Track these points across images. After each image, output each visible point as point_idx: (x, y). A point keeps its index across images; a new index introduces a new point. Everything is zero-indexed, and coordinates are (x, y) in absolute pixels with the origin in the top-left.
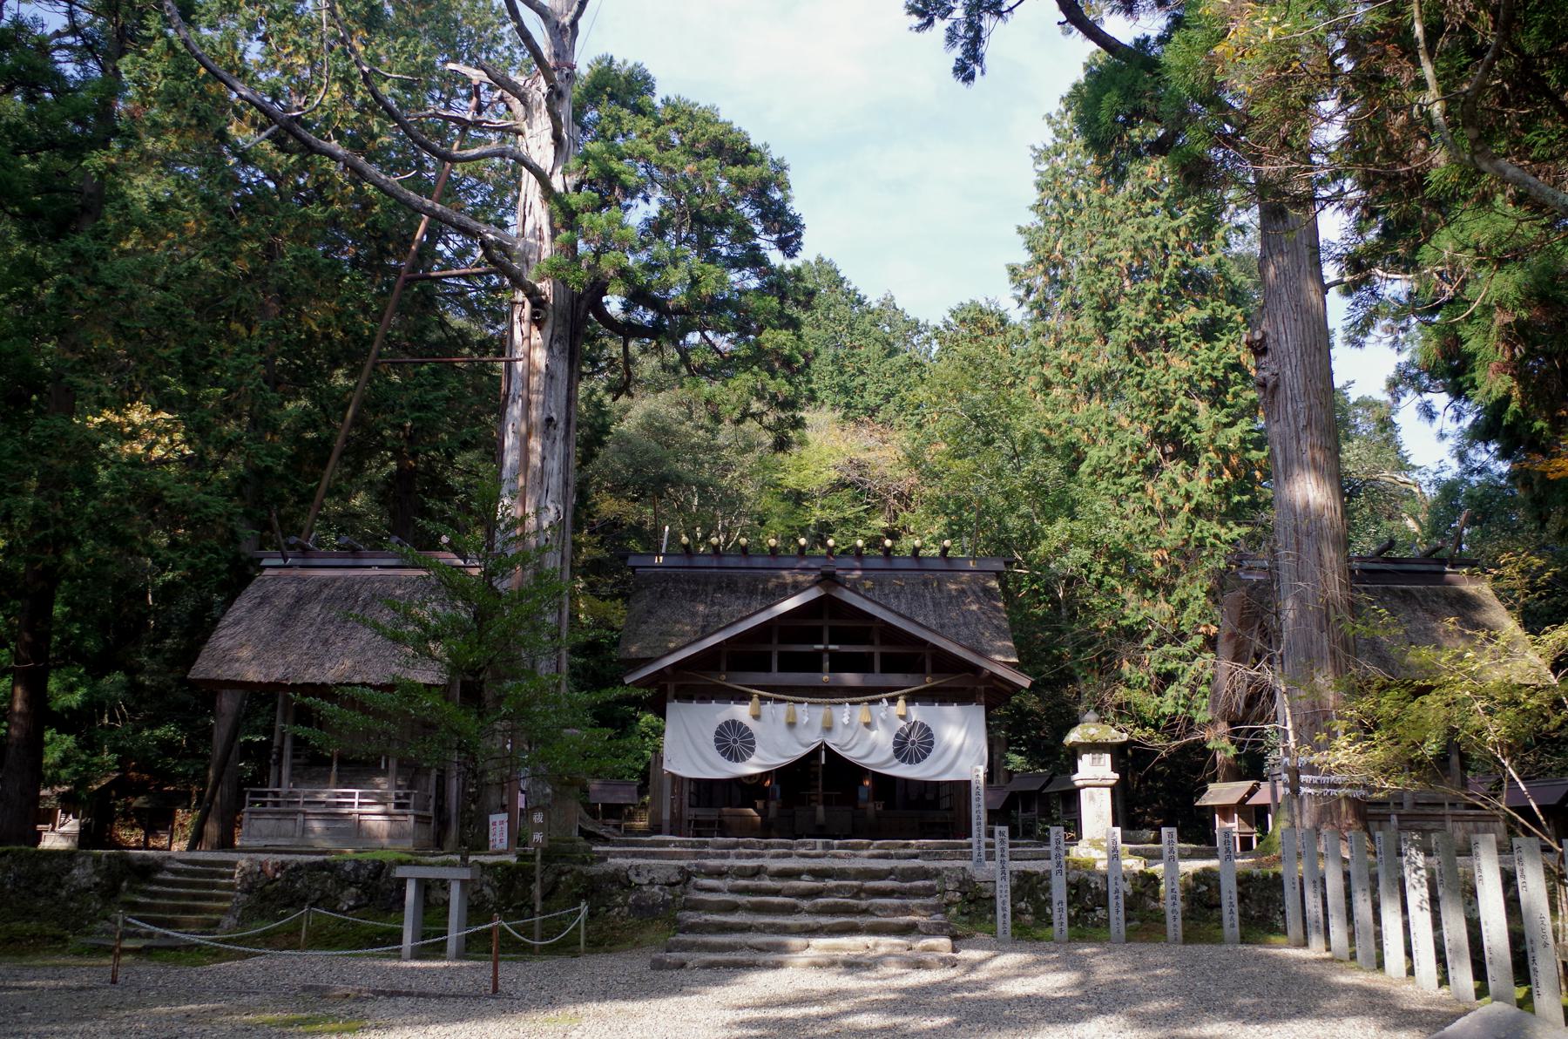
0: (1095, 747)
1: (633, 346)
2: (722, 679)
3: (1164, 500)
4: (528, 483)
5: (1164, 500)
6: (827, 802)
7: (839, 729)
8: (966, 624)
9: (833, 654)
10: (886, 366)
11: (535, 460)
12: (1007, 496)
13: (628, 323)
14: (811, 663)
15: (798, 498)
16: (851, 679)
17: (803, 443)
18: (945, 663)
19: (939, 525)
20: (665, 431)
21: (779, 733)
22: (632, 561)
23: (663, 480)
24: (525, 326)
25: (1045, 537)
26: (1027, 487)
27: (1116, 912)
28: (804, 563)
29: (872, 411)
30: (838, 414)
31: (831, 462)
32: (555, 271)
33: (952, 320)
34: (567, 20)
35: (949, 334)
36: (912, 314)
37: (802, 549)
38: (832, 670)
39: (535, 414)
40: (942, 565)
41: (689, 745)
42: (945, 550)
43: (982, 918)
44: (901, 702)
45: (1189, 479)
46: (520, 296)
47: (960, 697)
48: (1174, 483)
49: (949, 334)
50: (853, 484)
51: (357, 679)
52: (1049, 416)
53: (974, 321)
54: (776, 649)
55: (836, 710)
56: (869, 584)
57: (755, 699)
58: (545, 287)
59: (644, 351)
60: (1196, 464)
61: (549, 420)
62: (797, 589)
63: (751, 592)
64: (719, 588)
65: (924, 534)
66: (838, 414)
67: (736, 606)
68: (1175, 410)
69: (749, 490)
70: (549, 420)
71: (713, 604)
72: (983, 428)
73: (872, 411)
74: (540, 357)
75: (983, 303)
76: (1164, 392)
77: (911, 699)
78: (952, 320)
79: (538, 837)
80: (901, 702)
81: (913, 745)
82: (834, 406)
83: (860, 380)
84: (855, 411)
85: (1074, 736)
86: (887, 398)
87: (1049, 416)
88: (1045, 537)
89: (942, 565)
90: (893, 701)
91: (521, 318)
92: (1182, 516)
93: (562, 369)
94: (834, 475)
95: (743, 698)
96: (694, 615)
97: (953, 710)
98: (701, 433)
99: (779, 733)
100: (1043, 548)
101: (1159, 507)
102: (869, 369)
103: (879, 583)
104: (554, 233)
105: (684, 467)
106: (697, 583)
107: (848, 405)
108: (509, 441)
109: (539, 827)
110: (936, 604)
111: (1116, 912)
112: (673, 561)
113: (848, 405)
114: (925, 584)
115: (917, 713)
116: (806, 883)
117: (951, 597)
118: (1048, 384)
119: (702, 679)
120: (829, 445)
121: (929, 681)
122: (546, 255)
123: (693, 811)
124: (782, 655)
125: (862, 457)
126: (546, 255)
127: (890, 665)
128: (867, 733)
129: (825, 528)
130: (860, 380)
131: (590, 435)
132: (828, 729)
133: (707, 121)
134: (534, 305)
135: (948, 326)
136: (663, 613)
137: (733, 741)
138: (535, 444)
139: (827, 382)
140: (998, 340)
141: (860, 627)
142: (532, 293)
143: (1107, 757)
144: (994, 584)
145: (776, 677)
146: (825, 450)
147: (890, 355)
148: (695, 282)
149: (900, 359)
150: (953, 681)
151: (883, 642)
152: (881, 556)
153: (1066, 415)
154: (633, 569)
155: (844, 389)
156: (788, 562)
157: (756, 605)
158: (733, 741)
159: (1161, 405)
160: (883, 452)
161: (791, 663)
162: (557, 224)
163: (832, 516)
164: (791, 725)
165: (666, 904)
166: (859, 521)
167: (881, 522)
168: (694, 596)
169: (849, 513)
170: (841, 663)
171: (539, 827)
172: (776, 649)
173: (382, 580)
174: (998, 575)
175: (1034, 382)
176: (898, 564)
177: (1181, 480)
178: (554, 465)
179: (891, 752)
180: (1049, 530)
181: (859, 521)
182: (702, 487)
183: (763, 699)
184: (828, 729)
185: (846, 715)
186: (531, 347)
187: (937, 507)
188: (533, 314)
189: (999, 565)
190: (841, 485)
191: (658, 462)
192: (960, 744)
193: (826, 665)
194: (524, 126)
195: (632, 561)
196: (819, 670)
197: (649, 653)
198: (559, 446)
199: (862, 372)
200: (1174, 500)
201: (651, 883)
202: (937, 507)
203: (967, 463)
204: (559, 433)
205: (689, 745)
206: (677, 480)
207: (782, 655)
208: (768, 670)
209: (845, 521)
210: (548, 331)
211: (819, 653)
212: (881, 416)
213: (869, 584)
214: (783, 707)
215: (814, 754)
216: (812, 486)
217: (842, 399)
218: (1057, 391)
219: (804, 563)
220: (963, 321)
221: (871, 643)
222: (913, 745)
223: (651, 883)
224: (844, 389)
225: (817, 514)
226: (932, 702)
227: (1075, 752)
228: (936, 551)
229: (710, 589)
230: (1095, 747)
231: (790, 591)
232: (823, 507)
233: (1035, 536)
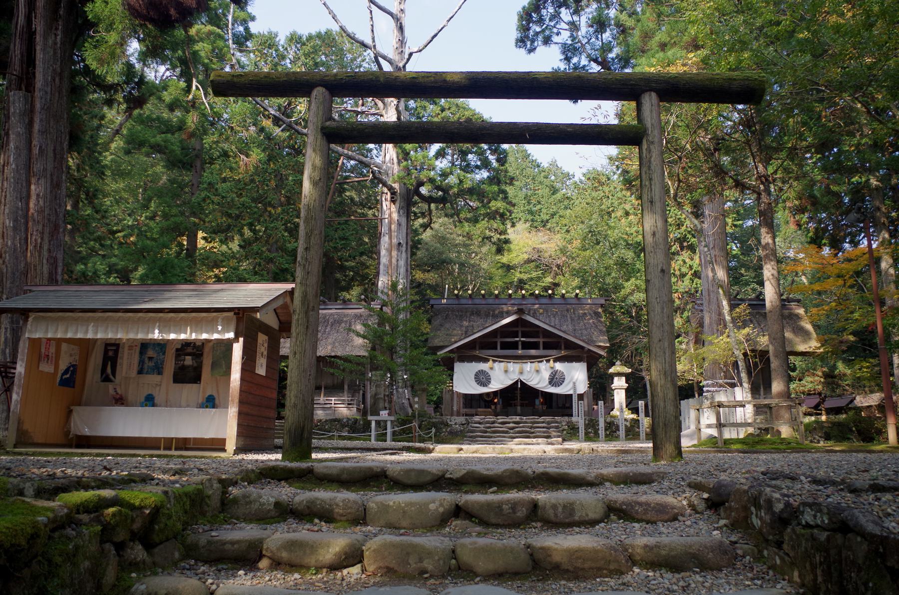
0: (619, 374)
1: (433, 206)
2: (477, 353)
3: (680, 270)
4: (391, 268)
5: (680, 270)
6: (522, 405)
7: (525, 373)
8: (586, 329)
9: (523, 342)
10: (551, 200)
11: (394, 261)
12: (606, 268)
13: (430, 197)
14: (514, 346)
15: (508, 268)
16: (533, 352)
17: (509, 250)
18: (569, 345)
19: (576, 282)
20: (443, 238)
21: (502, 375)
22: (432, 302)
23: (444, 262)
24: (388, 203)
25: (624, 288)
26: (616, 264)
27: (622, 433)
28: (512, 302)
29: (544, 223)
30: (528, 225)
31: (525, 250)
32: (401, 179)
33: (583, 178)
34: (401, 65)
35: (581, 186)
36: (566, 169)
37: (510, 295)
38: (523, 349)
39: (395, 241)
40: (575, 301)
41: (465, 380)
42: (577, 294)
43: (575, 435)
44: (552, 361)
45: (692, 259)
46: (386, 190)
47: (577, 359)
48: (684, 262)
49: (581, 186)
50: (536, 261)
51: (333, 354)
52: (627, 229)
53: (594, 179)
54: (499, 341)
55: (524, 365)
56: (541, 311)
57: (491, 361)
58: (396, 186)
59: (437, 209)
60: (694, 252)
61: (400, 244)
62: (509, 314)
63: (487, 315)
64: (472, 314)
65: (569, 286)
66: (528, 225)
67: (480, 321)
68: (684, 228)
69: (484, 265)
70: (400, 244)
71: (470, 321)
72: (594, 238)
73: (544, 223)
74: (395, 216)
75: (599, 169)
76: (679, 219)
77: (555, 360)
78: (583, 178)
79: (416, 406)
80: (552, 361)
81: (556, 379)
82: (526, 221)
83: (539, 207)
84: (538, 224)
85: (611, 370)
86: (553, 215)
87: (627, 229)
88: (624, 288)
89: (575, 301)
90: (548, 361)
91: (386, 200)
92: (688, 277)
93: (404, 221)
94: (526, 256)
95: (486, 360)
96: (462, 326)
97: (575, 365)
98: (461, 238)
99: (502, 375)
100: (623, 292)
101: (677, 273)
102: (543, 201)
103: (546, 311)
104: (399, 162)
105: (453, 256)
106: (462, 311)
107: (532, 220)
108: (383, 252)
109: (417, 403)
110: (572, 320)
111: (622, 433)
112: (450, 302)
113: (532, 220)
114: (567, 310)
115: (559, 366)
116: (512, 425)
117: (579, 317)
118: (627, 214)
119: (469, 353)
120: (523, 240)
121: (563, 353)
122: (396, 171)
123: (465, 410)
124: (502, 343)
125: (539, 246)
126: (396, 171)
127: (547, 346)
128: (537, 374)
129: (521, 283)
130: (539, 207)
131: (414, 245)
132: (521, 373)
133: (464, 108)
134: (392, 194)
135: (581, 182)
136: (447, 325)
137: (482, 378)
138: (394, 253)
139: (522, 208)
140: (606, 189)
141: (536, 331)
142: (390, 189)
143: (624, 378)
144: (600, 310)
145: (499, 352)
146: (521, 244)
147: (553, 194)
148: (461, 181)
149: (558, 196)
150: (572, 352)
151: (543, 337)
152: (548, 296)
153: (635, 228)
154: (432, 306)
155: (531, 212)
156: (504, 301)
157: (489, 321)
158: (482, 378)
159: (678, 225)
160: (549, 244)
161: (505, 346)
162: (400, 157)
163: (525, 277)
164: (506, 371)
165: (461, 431)
166: (539, 279)
167: (549, 280)
168: (461, 318)
169: (534, 274)
170: (526, 346)
171: (417, 403)
172: (499, 341)
173: (337, 314)
174: (602, 306)
175: (620, 213)
176: (555, 301)
177: (687, 260)
178: (402, 263)
179: (547, 382)
180: (626, 284)
181: (539, 279)
182: (462, 265)
183: (494, 361)
184: (521, 373)
185: (528, 366)
186: (390, 211)
187: (575, 273)
188: (392, 198)
189: (603, 301)
190: (529, 261)
191: (441, 253)
192: (576, 378)
193: (520, 347)
194: (384, 113)
195: (432, 302)
196: (517, 349)
197: (442, 344)
198: (404, 255)
199: (539, 203)
200: (684, 270)
201: (456, 424)
202: (575, 273)
203: (588, 253)
204: (404, 249)
205: (465, 380)
206: (451, 262)
207: (502, 343)
208: (496, 349)
209: (531, 279)
210: (398, 204)
211: (517, 342)
212: (549, 225)
213: (541, 311)
214: (502, 364)
215: (517, 382)
216: (515, 262)
217: (530, 217)
218: (631, 217)
219: (512, 302)
220: (589, 179)
221: (538, 337)
222: (556, 379)
223: (456, 424)
224: (531, 212)
225: (517, 276)
226: (572, 362)
227: (611, 377)
228: (573, 295)
229: (468, 314)
230: (619, 374)
231: (505, 315)
232: (521, 272)
233: (618, 288)
